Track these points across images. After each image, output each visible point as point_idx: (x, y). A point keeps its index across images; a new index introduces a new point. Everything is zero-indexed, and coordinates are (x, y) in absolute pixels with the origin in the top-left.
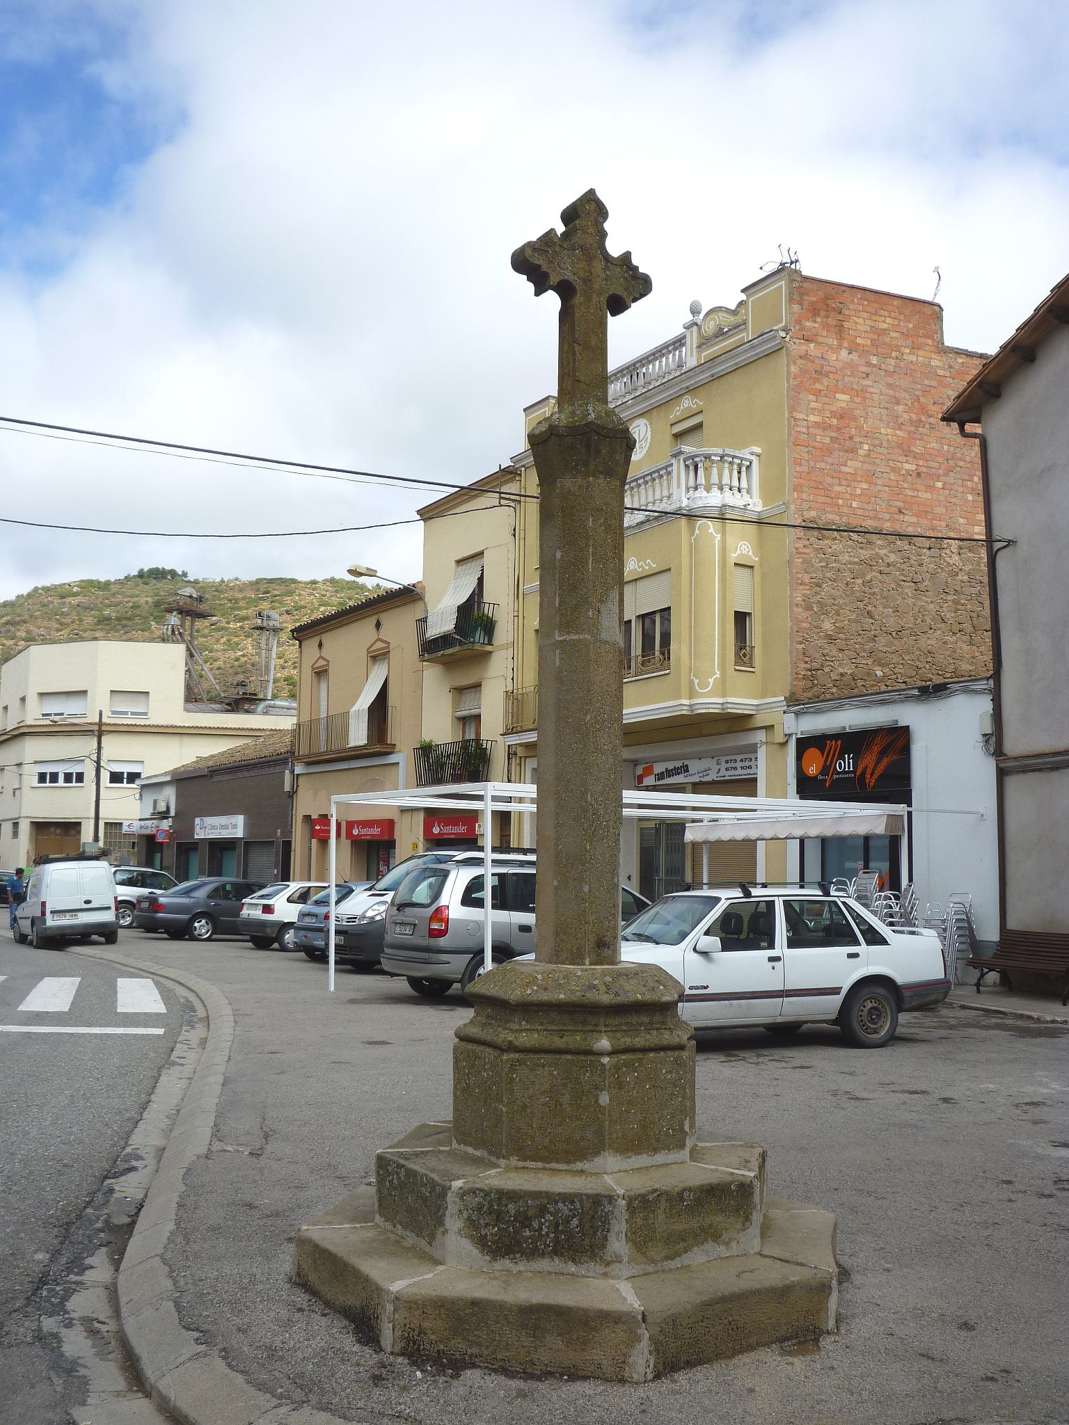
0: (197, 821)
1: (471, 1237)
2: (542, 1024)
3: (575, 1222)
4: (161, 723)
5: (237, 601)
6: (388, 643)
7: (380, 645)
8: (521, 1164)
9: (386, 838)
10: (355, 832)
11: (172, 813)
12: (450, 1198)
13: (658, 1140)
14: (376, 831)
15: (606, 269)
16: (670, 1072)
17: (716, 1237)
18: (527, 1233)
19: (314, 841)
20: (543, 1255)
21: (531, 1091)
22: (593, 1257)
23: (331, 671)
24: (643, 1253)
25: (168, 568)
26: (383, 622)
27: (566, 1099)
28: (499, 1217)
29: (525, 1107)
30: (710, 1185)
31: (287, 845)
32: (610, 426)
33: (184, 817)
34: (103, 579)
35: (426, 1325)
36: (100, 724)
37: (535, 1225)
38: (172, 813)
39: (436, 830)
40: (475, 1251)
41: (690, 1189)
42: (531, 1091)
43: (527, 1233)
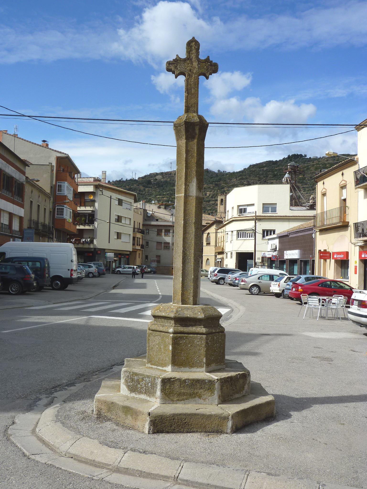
0: (285, 252)
1: (126, 385)
2: (160, 322)
3: (150, 384)
4: (283, 215)
5: (326, 164)
6: (346, 181)
7: (343, 182)
8: (151, 366)
9: (345, 259)
10: (335, 256)
11: (278, 249)
12: (122, 373)
13: (193, 364)
14: (342, 256)
15: (198, 64)
16: (198, 342)
17: (200, 397)
18: (139, 386)
19: (322, 260)
20: (142, 393)
21: (154, 344)
22: (153, 396)
23: (327, 194)
24: (169, 398)
25: (299, 153)
26: (344, 173)
27: (162, 347)
28: (133, 380)
29: (152, 348)
30: (197, 379)
31: (314, 261)
32: (192, 121)
33: (281, 252)
34: (274, 160)
35: (102, 407)
36: (256, 216)
37: (141, 383)
38: (278, 249)
39: (363, 256)
40: (127, 390)
41: (188, 379)
42: (154, 344)
43: (139, 386)
